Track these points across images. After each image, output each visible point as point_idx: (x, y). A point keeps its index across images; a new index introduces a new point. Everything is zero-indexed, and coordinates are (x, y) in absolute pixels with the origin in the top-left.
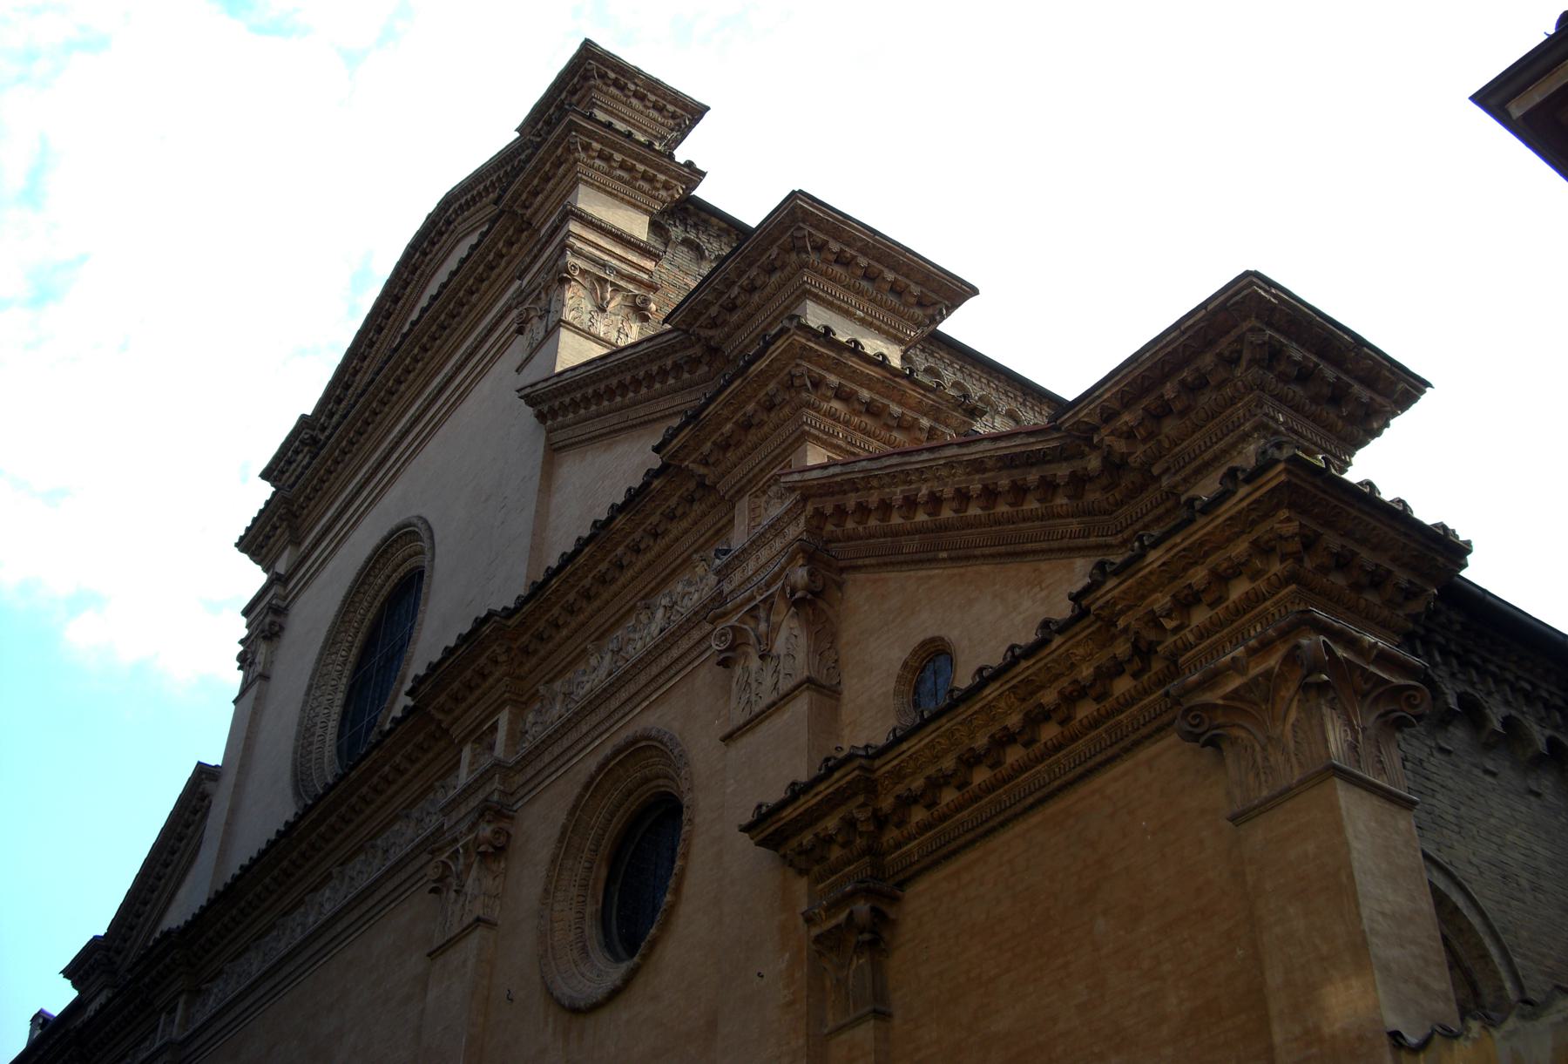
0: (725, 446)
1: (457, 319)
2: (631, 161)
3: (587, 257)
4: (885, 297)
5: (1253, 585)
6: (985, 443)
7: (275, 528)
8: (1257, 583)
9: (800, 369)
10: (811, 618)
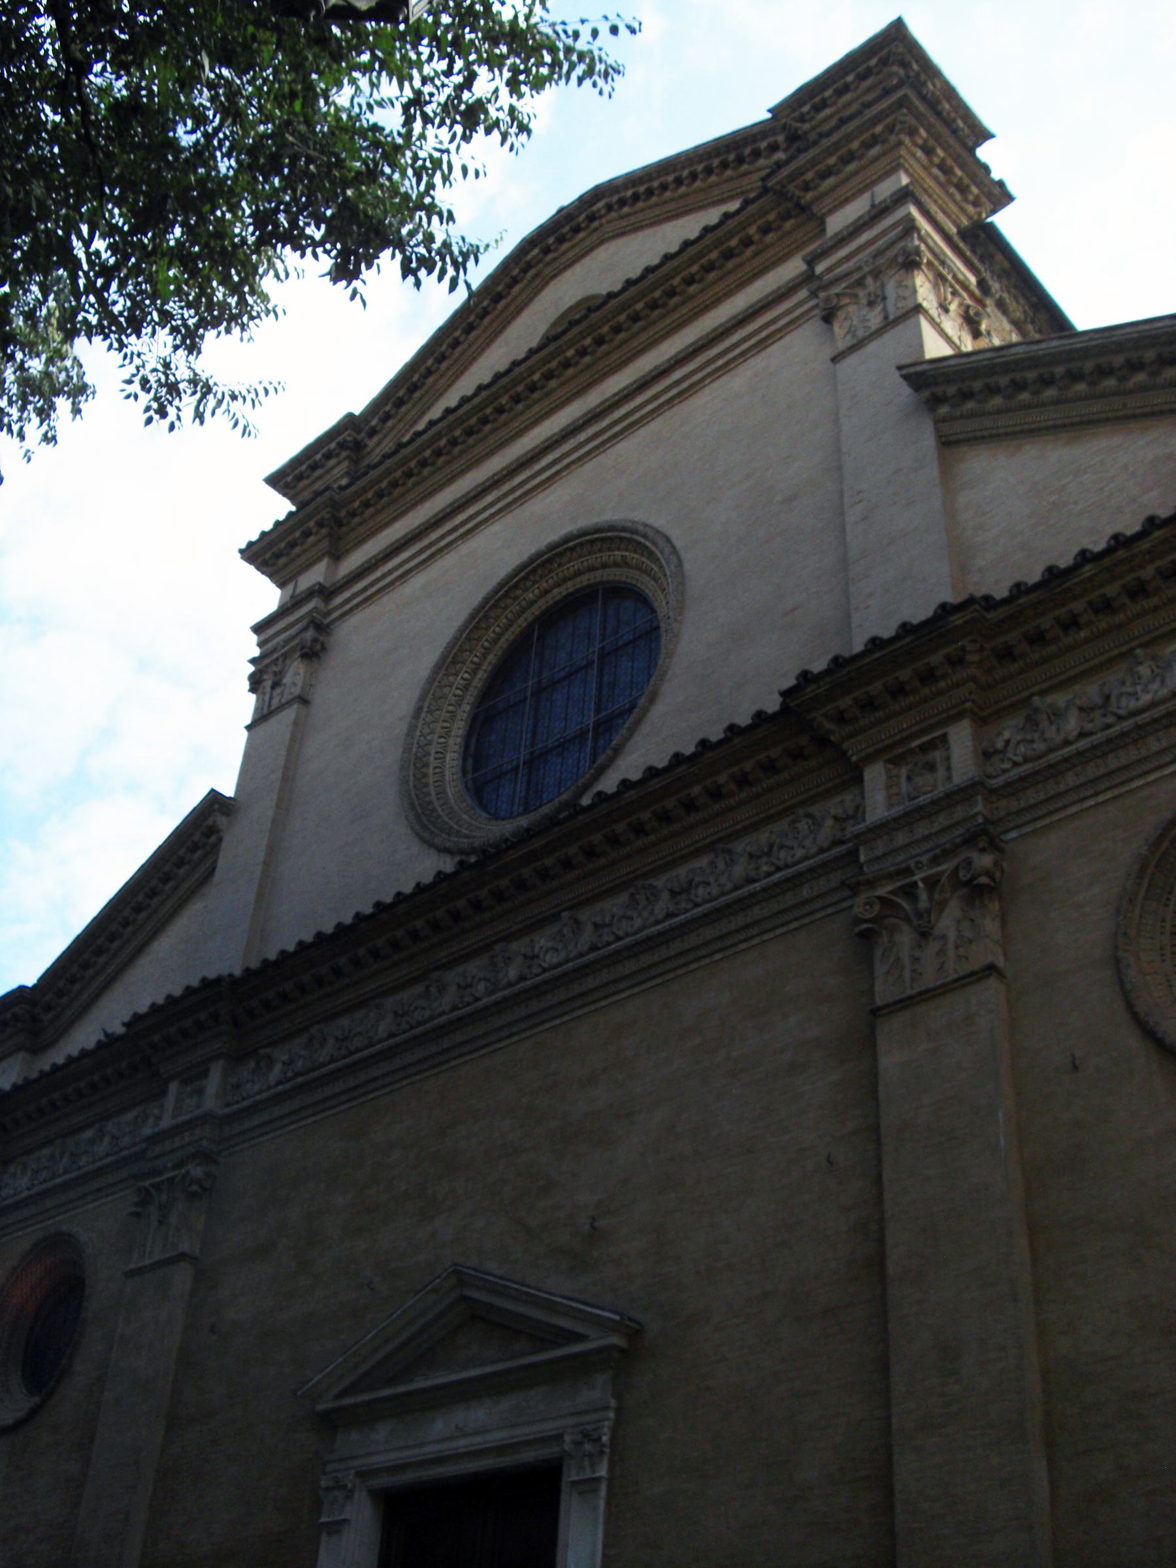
7: (307, 534)
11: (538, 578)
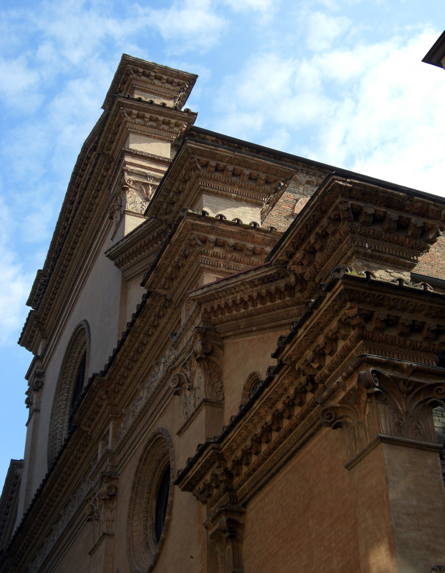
0: (171, 279)
1: (92, 212)
2: (155, 116)
3: (136, 174)
4: (247, 184)
5: (345, 342)
6: (252, 272)
7: (34, 332)
8: (347, 341)
9: (193, 236)
10: (207, 367)
11: (75, 347)
